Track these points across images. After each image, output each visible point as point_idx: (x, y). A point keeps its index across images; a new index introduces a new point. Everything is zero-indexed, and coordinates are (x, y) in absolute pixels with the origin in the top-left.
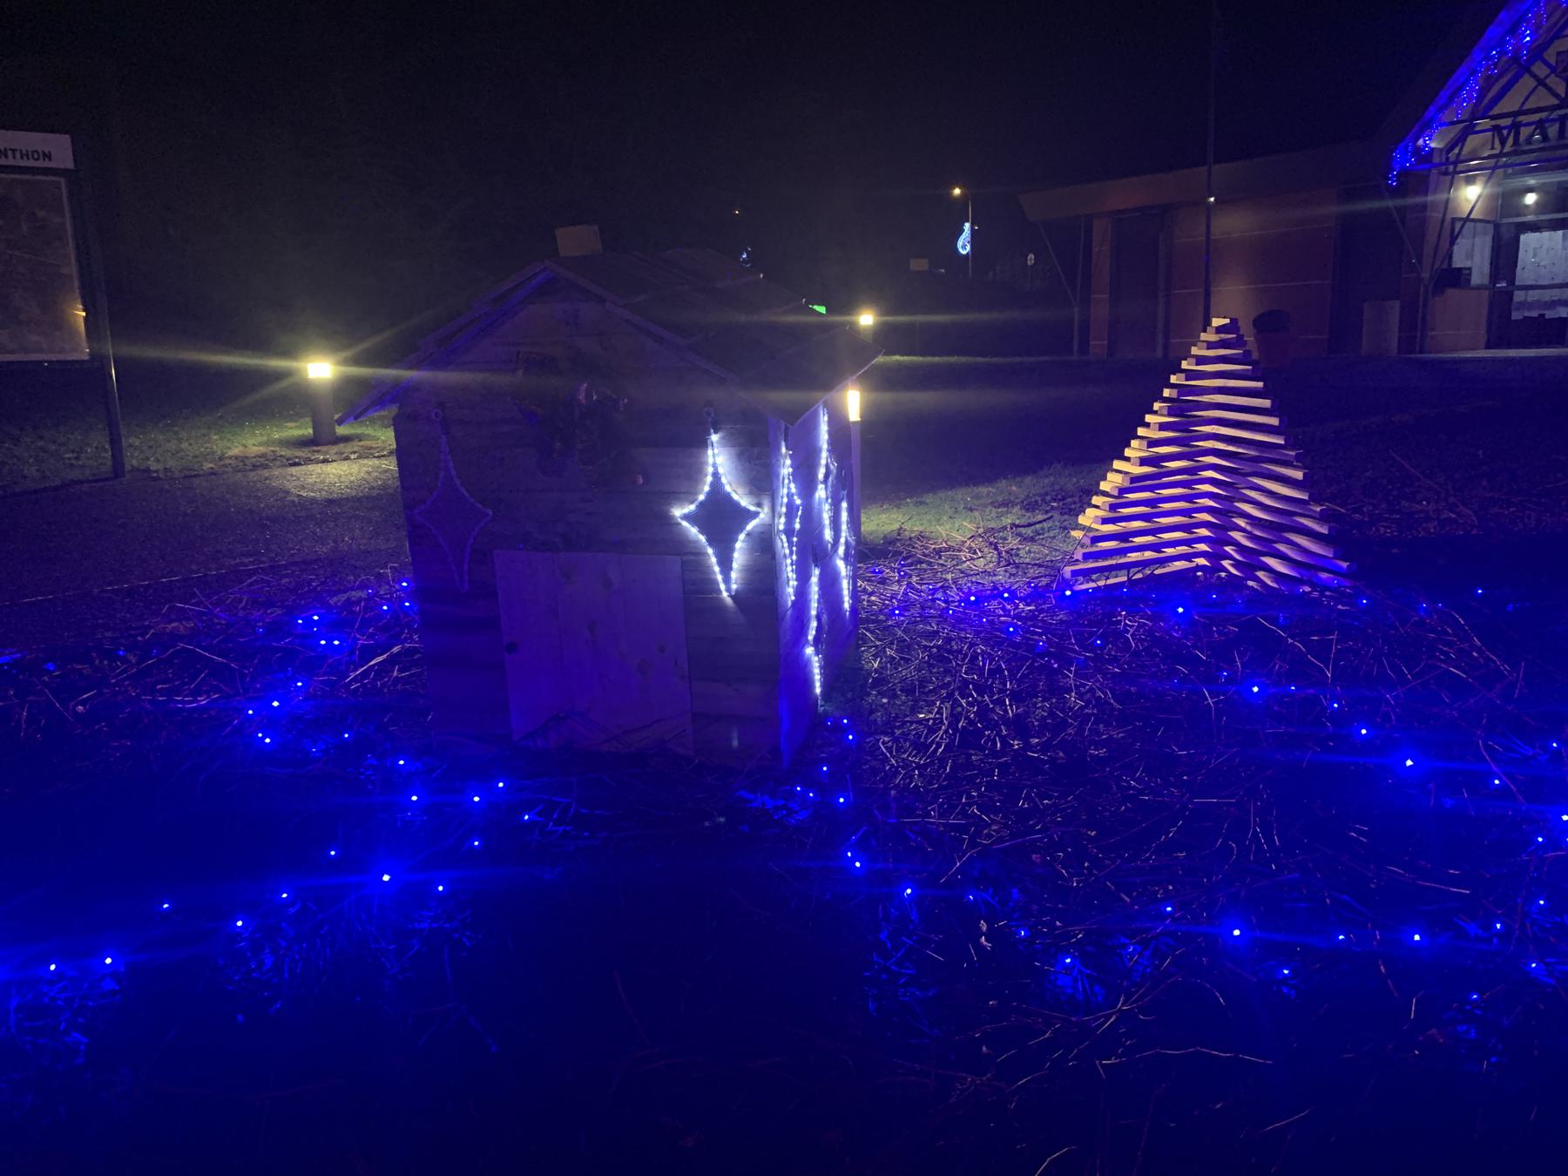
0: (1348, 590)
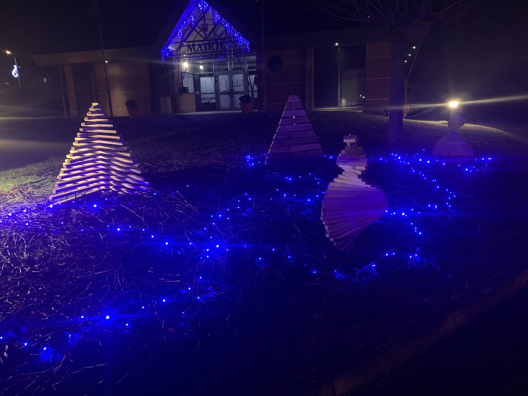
0: (149, 191)
